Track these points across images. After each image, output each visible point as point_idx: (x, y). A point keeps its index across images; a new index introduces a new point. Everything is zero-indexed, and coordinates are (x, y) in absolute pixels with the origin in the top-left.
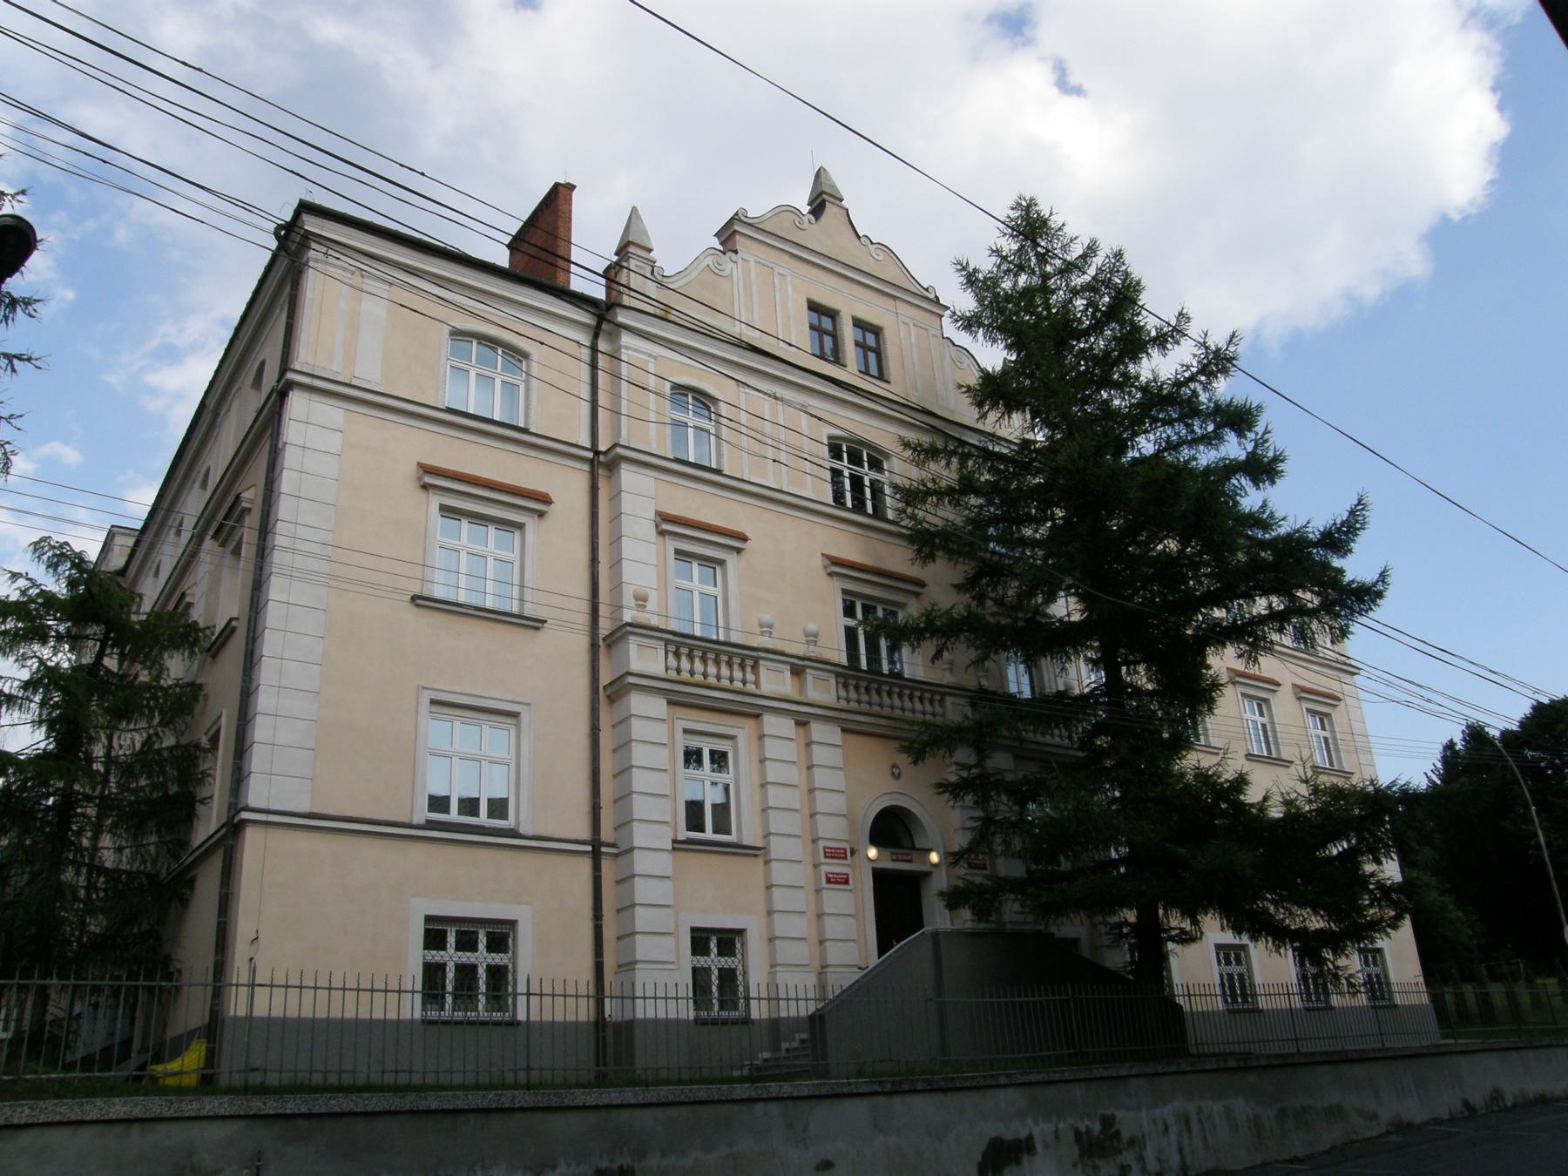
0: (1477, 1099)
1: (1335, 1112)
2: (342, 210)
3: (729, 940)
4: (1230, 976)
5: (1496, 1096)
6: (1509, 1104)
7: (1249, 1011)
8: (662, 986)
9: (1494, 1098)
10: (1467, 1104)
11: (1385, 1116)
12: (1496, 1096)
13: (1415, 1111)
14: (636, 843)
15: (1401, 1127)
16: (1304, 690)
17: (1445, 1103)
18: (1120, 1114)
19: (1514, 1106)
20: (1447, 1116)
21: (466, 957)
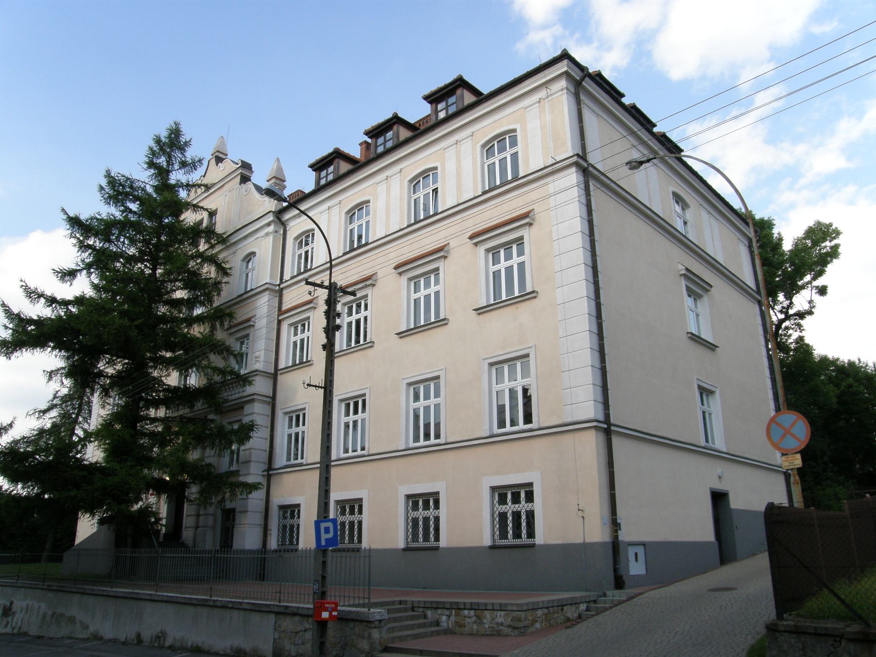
0: (146, 636)
1: (72, 620)
2: (435, 132)
3: (431, 500)
4: (415, 521)
5: (161, 636)
6: (167, 644)
7: (353, 550)
8: (468, 524)
9: (158, 637)
10: (139, 636)
11: (92, 629)
12: (161, 636)
13: (107, 631)
14: (251, 472)
15: (97, 637)
16: (437, 192)
17: (126, 631)
18: (15, 602)
19: (170, 647)
20: (123, 640)
21: (516, 507)
